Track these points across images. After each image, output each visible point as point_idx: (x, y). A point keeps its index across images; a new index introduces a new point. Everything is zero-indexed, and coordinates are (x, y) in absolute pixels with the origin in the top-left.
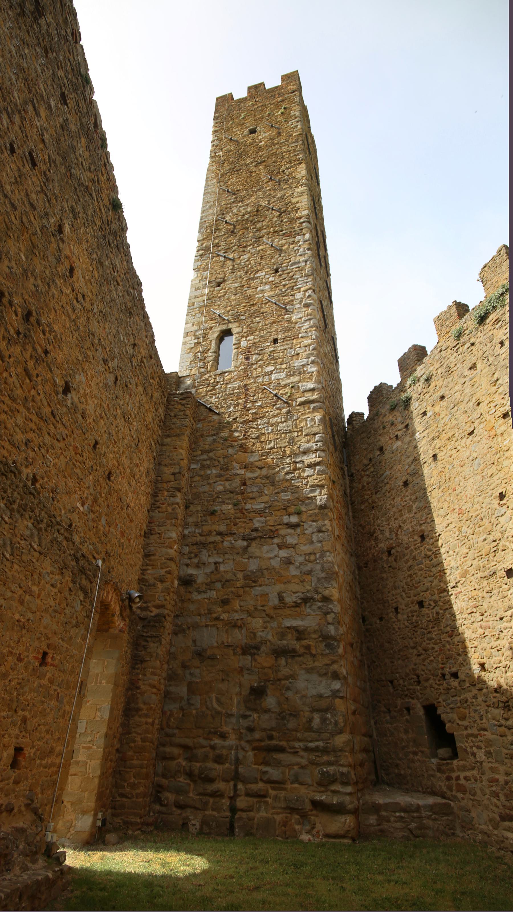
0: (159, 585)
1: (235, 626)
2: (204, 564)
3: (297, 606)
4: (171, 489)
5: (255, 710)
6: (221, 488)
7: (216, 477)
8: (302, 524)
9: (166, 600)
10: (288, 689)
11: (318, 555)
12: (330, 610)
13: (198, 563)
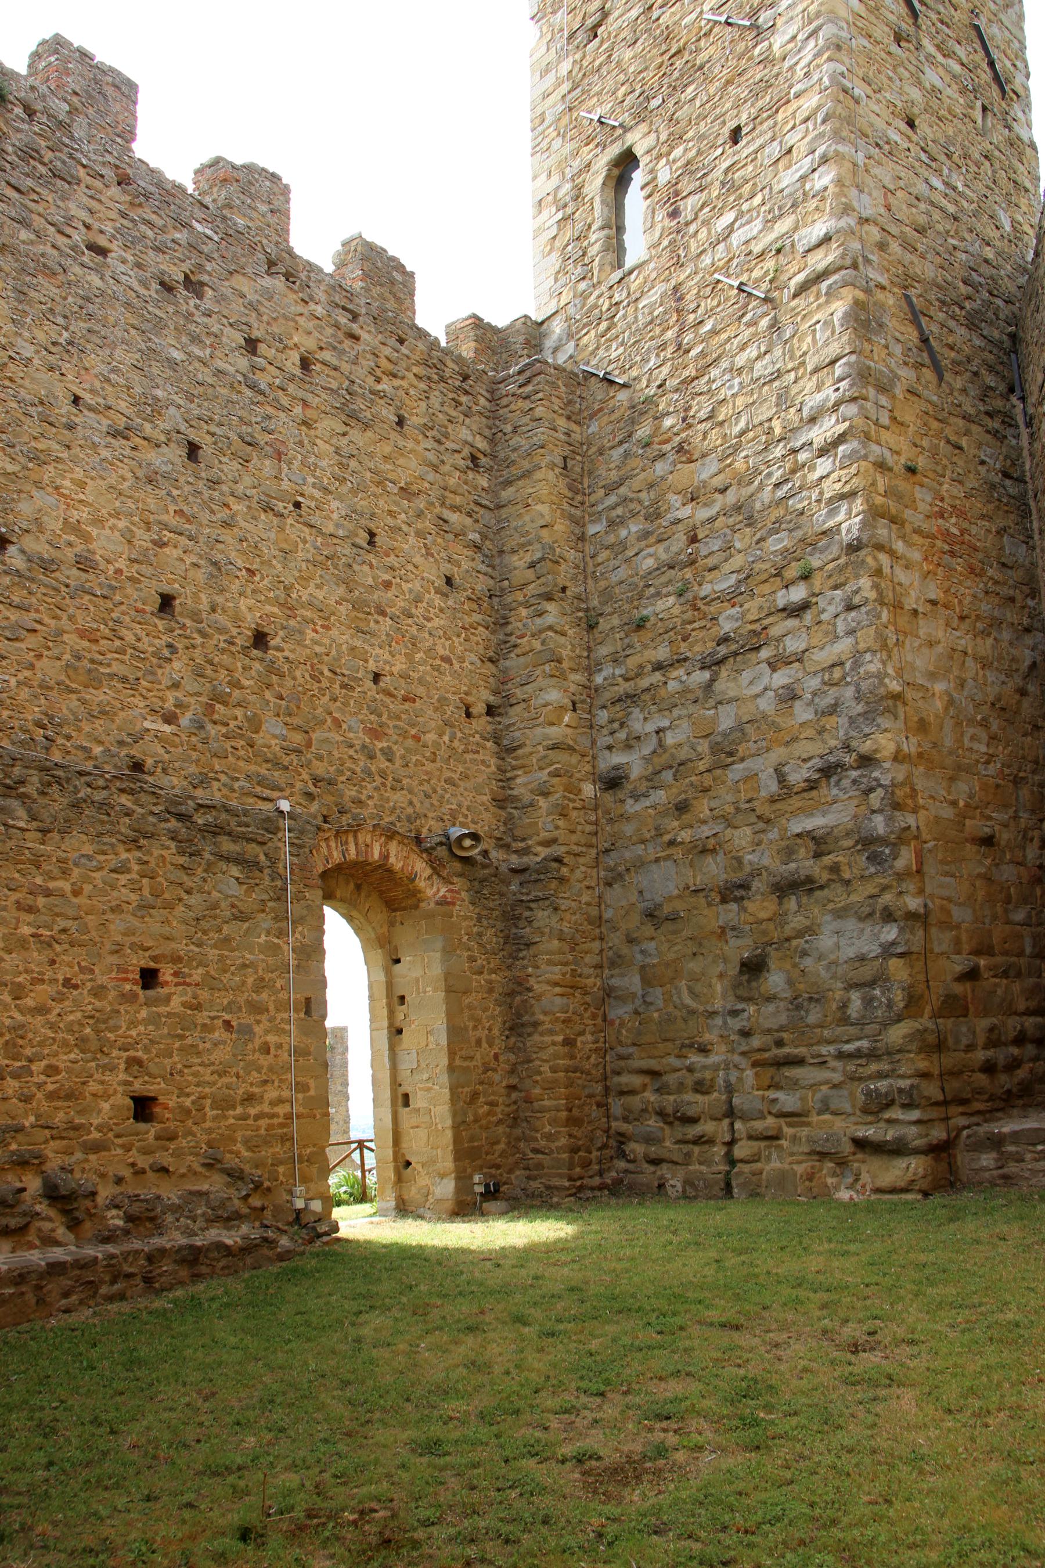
0: (542, 802)
1: (704, 851)
2: (638, 738)
3: (812, 788)
4: (533, 601)
5: (749, 999)
6: (650, 562)
7: (638, 540)
8: (814, 600)
9: (557, 828)
10: (804, 954)
11: (848, 666)
12: (874, 783)
13: (627, 739)
